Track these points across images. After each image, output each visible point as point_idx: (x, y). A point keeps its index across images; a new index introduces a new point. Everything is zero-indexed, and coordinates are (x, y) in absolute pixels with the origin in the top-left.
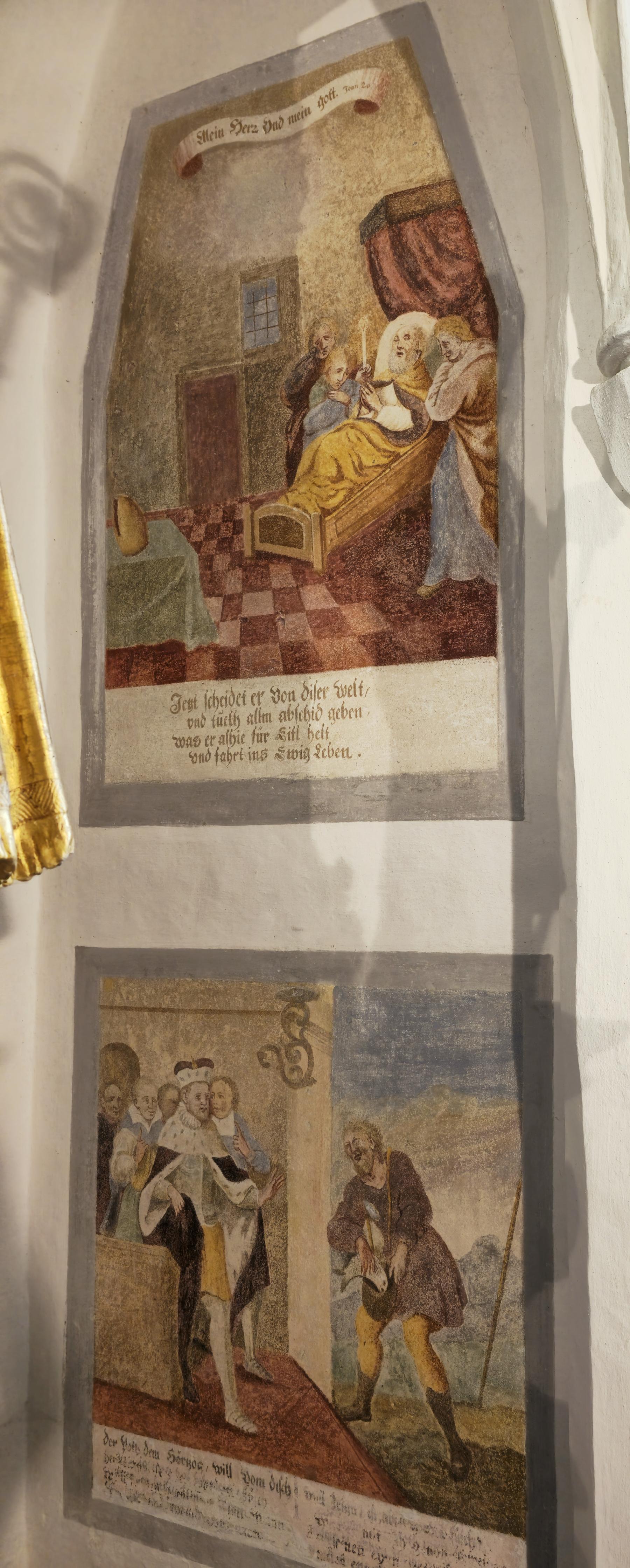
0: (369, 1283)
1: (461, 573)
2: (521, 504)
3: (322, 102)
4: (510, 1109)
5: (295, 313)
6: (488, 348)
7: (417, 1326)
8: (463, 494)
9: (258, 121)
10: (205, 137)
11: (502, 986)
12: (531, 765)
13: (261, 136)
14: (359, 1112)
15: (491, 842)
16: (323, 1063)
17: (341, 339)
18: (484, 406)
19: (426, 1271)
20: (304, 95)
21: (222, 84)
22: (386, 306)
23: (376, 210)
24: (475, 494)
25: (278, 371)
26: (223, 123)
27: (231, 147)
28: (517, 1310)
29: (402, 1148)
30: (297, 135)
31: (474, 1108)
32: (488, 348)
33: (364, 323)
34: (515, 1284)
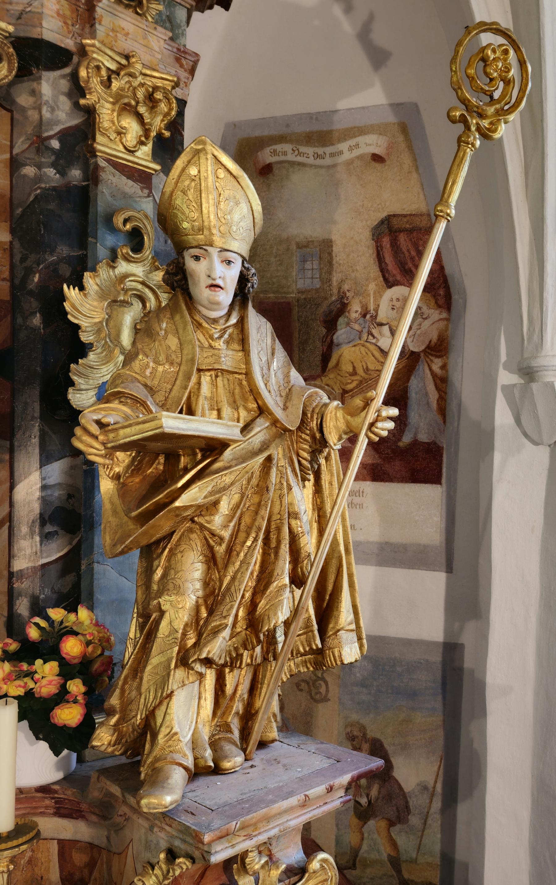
0: (357, 802)
1: (423, 437)
2: (460, 405)
3: (351, 149)
4: (438, 719)
5: (330, 273)
6: (444, 315)
7: (383, 824)
8: (427, 394)
9: (310, 150)
10: (274, 153)
11: (437, 658)
12: (459, 544)
13: (311, 161)
14: (354, 717)
15: (433, 584)
16: (334, 691)
17: (357, 294)
18: (439, 348)
19: (389, 798)
20: (340, 141)
21: (287, 121)
22: (386, 280)
23: (382, 222)
24: (433, 395)
25: (318, 305)
26: (287, 147)
27: (292, 164)
28: (438, 817)
29: (378, 736)
30: (334, 166)
31: (419, 718)
32: (444, 315)
33: (372, 287)
34: (437, 804)
